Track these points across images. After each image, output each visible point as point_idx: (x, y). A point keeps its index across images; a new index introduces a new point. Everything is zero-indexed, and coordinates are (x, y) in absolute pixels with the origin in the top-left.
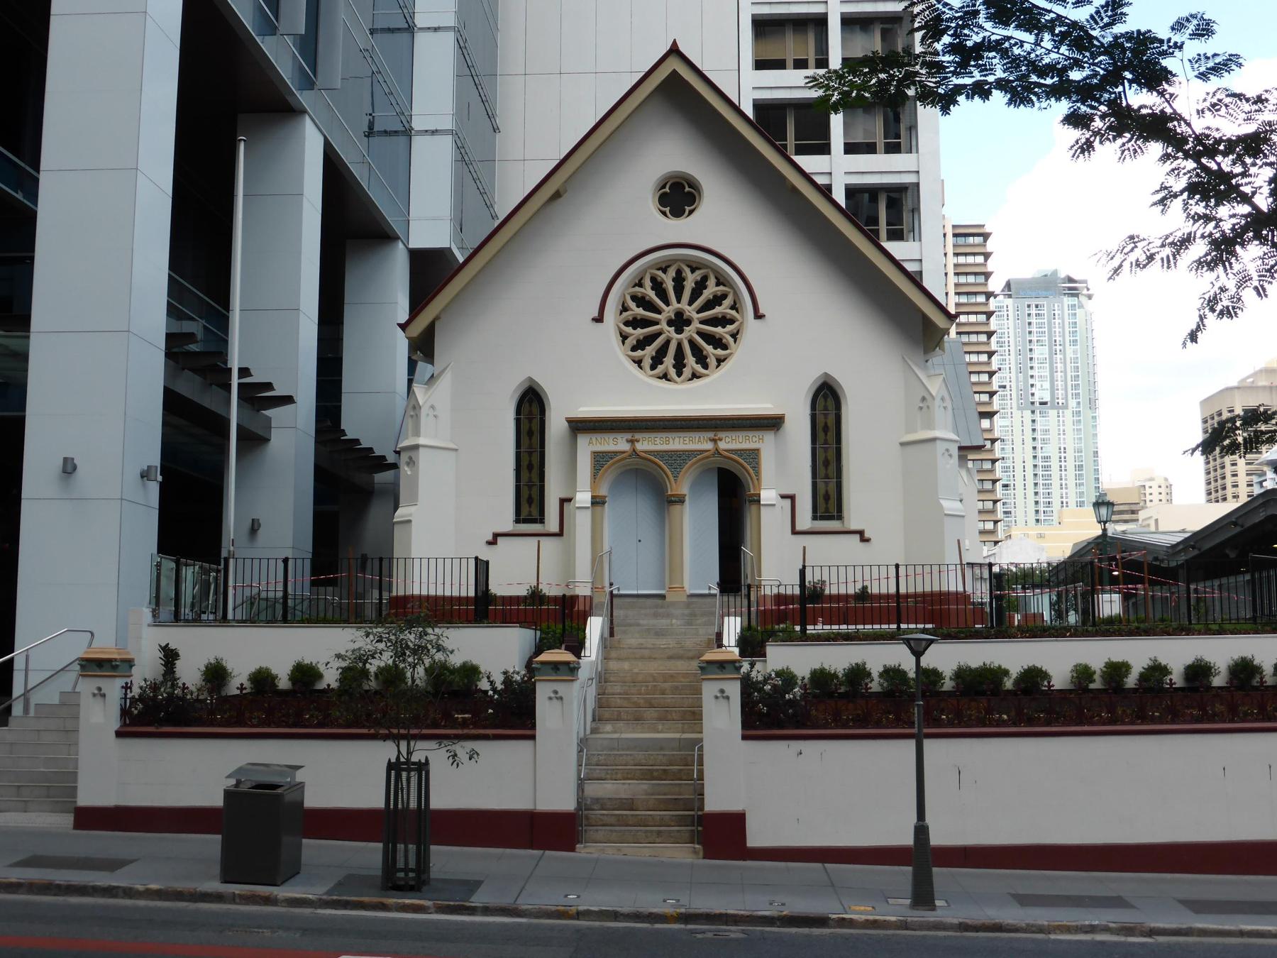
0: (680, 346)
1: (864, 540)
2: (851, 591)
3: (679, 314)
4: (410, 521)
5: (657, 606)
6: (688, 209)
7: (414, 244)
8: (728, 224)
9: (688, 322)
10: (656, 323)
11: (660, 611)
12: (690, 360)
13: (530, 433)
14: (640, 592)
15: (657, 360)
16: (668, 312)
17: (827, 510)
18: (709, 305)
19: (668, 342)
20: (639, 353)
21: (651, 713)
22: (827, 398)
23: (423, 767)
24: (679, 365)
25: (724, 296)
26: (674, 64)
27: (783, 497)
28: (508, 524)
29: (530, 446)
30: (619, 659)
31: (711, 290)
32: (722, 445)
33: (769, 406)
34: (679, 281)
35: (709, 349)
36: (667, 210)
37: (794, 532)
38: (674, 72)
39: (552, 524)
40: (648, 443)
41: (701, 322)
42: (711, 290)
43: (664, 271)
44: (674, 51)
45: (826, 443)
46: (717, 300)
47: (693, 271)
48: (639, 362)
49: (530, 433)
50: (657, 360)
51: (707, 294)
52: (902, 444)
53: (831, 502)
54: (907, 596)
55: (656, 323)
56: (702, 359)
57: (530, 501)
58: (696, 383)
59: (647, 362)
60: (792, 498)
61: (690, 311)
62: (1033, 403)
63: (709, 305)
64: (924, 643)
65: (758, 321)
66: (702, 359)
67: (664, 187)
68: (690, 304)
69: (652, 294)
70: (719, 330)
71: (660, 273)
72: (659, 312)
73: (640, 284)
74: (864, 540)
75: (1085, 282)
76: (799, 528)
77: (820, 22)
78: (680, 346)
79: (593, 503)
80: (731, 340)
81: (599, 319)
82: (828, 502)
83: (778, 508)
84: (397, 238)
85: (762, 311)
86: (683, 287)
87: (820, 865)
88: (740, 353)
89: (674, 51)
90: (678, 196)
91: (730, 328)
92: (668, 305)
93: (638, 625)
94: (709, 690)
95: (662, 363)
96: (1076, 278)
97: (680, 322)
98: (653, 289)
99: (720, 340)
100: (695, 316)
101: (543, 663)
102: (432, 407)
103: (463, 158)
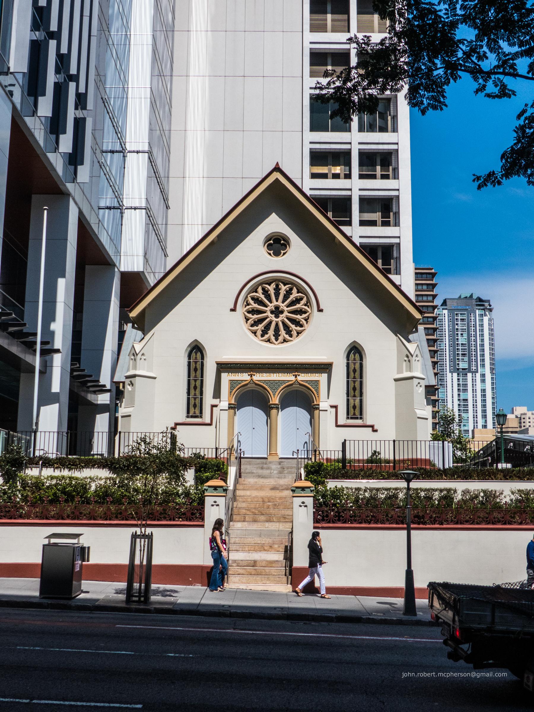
0: (277, 325)
2: (365, 458)
3: (277, 308)
4: (130, 416)
5: (263, 463)
6: (282, 252)
7: (122, 269)
8: (301, 260)
9: (282, 312)
11: (265, 466)
12: (283, 332)
13: (196, 370)
14: (254, 456)
15: (264, 332)
16: (271, 306)
17: (354, 414)
18: (292, 303)
19: (270, 323)
20: (255, 328)
21: (262, 518)
22: (355, 351)
23: (150, 537)
24: (277, 335)
25: (301, 299)
26: (277, 175)
27: (332, 407)
28: (182, 417)
30: (244, 490)
31: (295, 294)
32: (299, 378)
34: (266, 292)
35: (293, 327)
36: (271, 252)
37: (337, 426)
38: (277, 180)
39: (207, 419)
40: (258, 377)
41: (289, 312)
42: (295, 294)
44: (277, 169)
45: (354, 378)
46: (298, 301)
48: (255, 333)
49: (196, 370)
50: (264, 332)
51: (292, 297)
52: (396, 380)
53: (357, 410)
54: (399, 461)
56: (289, 332)
57: (194, 406)
58: (285, 345)
59: (259, 333)
60: (336, 407)
61: (283, 306)
62: (458, 369)
63: (292, 303)
64: (412, 476)
66: (289, 332)
68: (283, 302)
70: (298, 317)
72: (266, 306)
75: (488, 301)
76: (339, 423)
77: (347, 154)
78: (277, 325)
79: (229, 408)
80: (305, 322)
81: (233, 310)
82: (355, 410)
83: (328, 412)
85: (321, 307)
87: (353, 596)
88: (309, 329)
89: (277, 169)
90: (277, 244)
91: (304, 316)
92: (271, 302)
93: (253, 473)
94: (297, 501)
95: (267, 334)
96: (484, 299)
97: (277, 312)
99: (299, 322)
100: (286, 309)
101: (209, 487)
103: (151, 221)
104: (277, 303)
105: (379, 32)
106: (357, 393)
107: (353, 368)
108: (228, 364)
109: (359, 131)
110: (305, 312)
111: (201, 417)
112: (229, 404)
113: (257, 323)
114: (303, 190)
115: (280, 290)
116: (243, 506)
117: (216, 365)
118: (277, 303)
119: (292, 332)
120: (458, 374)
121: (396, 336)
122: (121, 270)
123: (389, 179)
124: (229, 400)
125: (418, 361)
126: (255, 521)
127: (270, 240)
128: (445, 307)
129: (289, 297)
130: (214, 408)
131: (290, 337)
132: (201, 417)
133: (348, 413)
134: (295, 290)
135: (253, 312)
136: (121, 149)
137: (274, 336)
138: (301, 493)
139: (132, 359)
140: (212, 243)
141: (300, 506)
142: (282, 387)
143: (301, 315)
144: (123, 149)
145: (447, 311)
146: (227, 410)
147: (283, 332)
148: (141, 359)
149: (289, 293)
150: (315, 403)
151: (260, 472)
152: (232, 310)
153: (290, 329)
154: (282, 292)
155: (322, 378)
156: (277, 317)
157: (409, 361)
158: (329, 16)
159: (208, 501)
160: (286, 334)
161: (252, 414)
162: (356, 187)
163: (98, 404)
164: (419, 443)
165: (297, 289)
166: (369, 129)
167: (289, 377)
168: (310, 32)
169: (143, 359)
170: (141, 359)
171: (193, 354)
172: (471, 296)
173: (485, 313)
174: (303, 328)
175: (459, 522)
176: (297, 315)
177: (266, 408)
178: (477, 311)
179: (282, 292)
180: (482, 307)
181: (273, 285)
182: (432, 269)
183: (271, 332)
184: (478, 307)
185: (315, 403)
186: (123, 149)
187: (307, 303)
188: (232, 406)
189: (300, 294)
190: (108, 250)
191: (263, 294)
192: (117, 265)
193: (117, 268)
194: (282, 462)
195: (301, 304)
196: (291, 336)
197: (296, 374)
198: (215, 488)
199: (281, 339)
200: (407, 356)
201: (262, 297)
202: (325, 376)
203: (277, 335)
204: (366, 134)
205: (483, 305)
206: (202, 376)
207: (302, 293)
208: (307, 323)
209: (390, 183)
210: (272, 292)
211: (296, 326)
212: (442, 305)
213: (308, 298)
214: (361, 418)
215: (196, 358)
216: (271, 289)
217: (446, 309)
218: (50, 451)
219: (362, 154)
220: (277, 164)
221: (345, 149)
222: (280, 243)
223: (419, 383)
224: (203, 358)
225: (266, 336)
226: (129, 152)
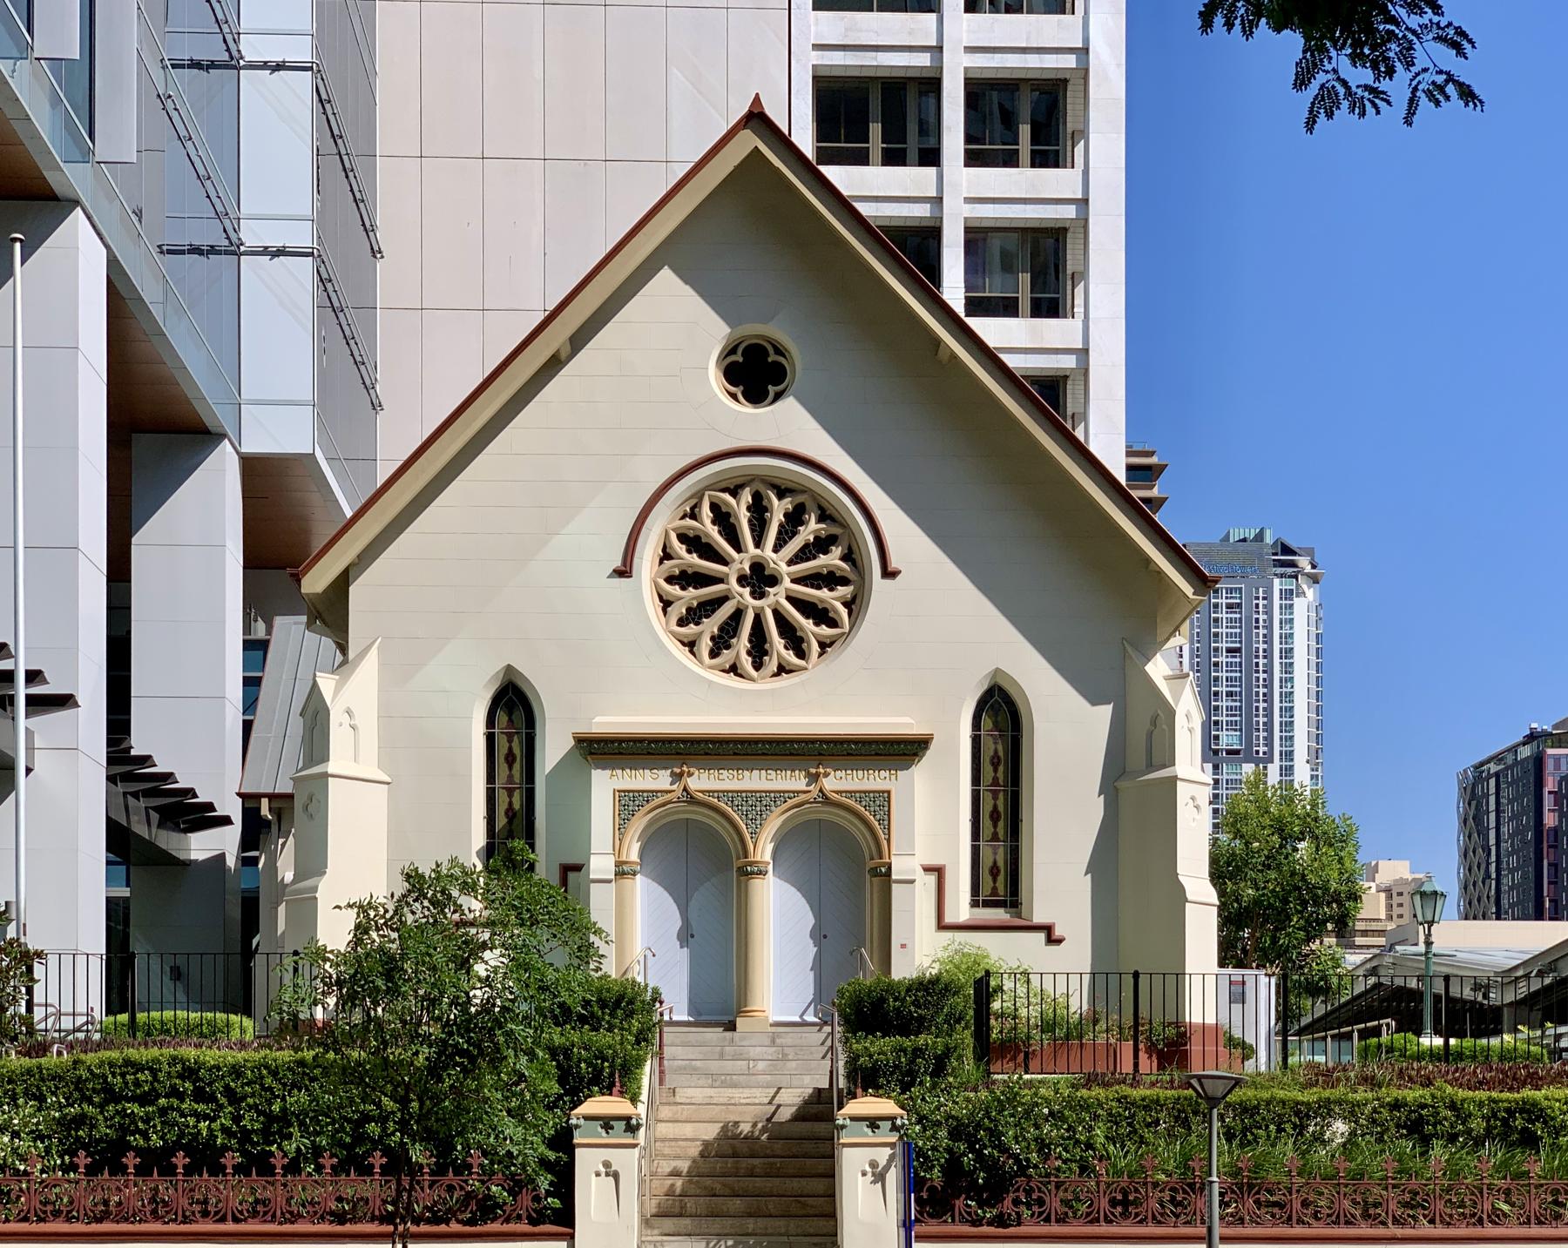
1: (1052, 940)
7: (246, 448)
9: (774, 581)
10: (758, 543)
16: (741, 563)
17: (994, 891)
18: (804, 554)
19: (738, 615)
22: (1001, 713)
27: (927, 869)
29: (510, 778)
36: (738, 358)
37: (942, 926)
40: (702, 781)
43: (734, 493)
47: (780, 497)
50: (721, 642)
55: (758, 543)
60: (938, 871)
61: (778, 562)
62: (1216, 752)
65: (888, 582)
67: (733, 351)
69: (713, 532)
70: (824, 593)
71: (727, 497)
73: (693, 515)
74: (1052, 940)
75: (1310, 552)
81: (624, 572)
84: (223, 436)
85: (894, 563)
96: (1293, 544)
98: (714, 522)
100: (787, 583)
102: (349, 712)
108: (813, 741)
109: (967, 11)
112: (618, 864)
120: (1216, 767)
122: (244, 450)
130: (571, 876)
135: (686, 579)
136: (226, 57)
138: (866, 1135)
146: (609, 881)
149: (830, 580)
151: (715, 1066)
156: (758, 594)
159: (587, 1162)
162: (965, 192)
163: (187, 864)
172: (1260, 537)
175: (1342, 1219)
176: (819, 588)
178: (1277, 581)
180: (1290, 570)
182: (1151, 454)
184: (1282, 570)
194: (779, 1035)
198: (607, 1122)
209: (1053, 331)
218: (67, 1007)
219: (978, 90)
220: (757, 99)
224: (530, 722)
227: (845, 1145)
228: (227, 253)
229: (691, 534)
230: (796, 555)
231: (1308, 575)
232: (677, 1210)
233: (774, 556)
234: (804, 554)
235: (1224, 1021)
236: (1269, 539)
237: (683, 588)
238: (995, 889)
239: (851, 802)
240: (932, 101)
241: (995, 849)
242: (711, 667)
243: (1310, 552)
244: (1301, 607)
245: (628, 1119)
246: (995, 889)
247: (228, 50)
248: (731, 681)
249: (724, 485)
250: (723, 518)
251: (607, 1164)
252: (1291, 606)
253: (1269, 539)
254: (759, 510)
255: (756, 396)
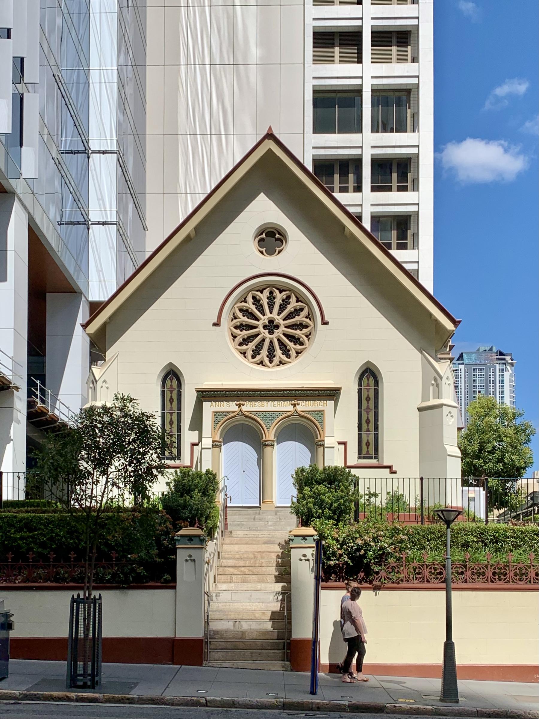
0: (271, 342)
3: (271, 321)
6: (278, 249)
8: (303, 259)
9: (277, 327)
12: (278, 352)
14: (244, 505)
15: (256, 352)
16: (264, 320)
17: (368, 452)
18: (290, 316)
19: (257, 319)
22: (369, 375)
24: (271, 356)
25: (302, 310)
27: (340, 443)
31: (293, 304)
32: (299, 408)
33: (331, 382)
38: (270, 151)
40: (249, 407)
42: (293, 304)
44: (270, 136)
46: (297, 312)
47: (281, 292)
50: (256, 352)
51: (290, 308)
52: (420, 409)
59: (250, 353)
61: (279, 319)
63: (290, 316)
66: (286, 351)
68: (279, 314)
73: (245, 301)
78: (271, 342)
79: (213, 446)
80: (306, 339)
85: (327, 319)
86: (261, 306)
89: (270, 136)
90: (271, 239)
97: (271, 326)
99: (299, 339)
100: (282, 322)
101: (182, 536)
104: (271, 315)
105: (398, 4)
106: (371, 426)
107: (366, 396)
110: (306, 327)
111: (179, 459)
112: (213, 441)
113: (246, 341)
114: (305, 165)
115: (274, 298)
116: (229, 564)
117: (195, 394)
118: (271, 315)
119: (290, 352)
121: (421, 353)
123: (407, 190)
124: (213, 436)
125: (449, 384)
126: (244, 582)
127: (262, 234)
128: (461, 362)
129: (286, 308)
130: (195, 447)
131: (287, 357)
132: (179, 459)
133: (360, 452)
134: (293, 299)
135: (242, 327)
137: (267, 356)
138: (301, 544)
139: (91, 388)
140: (188, 239)
141: (301, 560)
142: (278, 419)
143: (301, 330)
144: (86, 149)
145: (463, 366)
146: (210, 449)
147: (278, 352)
148: (102, 387)
149: (286, 302)
150: (319, 439)
151: (251, 523)
152: (215, 325)
153: (288, 347)
154: (278, 301)
155: (327, 406)
156: (271, 333)
157: (438, 385)
158: (337, 49)
160: (283, 354)
161: (240, 451)
164: (448, 481)
165: (296, 297)
166: (383, 130)
167: (286, 406)
168: (314, 5)
169: (104, 388)
170: (102, 387)
171: (168, 382)
172: (491, 349)
173: (506, 368)
174: (304, 347)
176: (296, 330)
177: (260, 445)
178: (497, 365)
179: (278, 301)
180: (503, 361)
181: (266, 293)
183: (264, 352)
185: (319, 439)
186: (86, 149)
187: (309, 314)
188: (217, 443)
189: (300, 303)
190: (50, 242)
191: (253, 304)
192: (83, 291)
193: (85, 297)
194: (278, 511)
195: (301, 316)
196: (289, 357)
197: (296, 402)
198: (190, 538)
199: (276, 360)
200: (435, 380)
201: (253, 308)
202: (331, 403)
203: (271, 356)
204: (380, 135)
205: (504, 359)
206: (180, 408)
207: (302, 302)
208: (309, 340)
210: (265, 302)
211: (295, 344)
212: (458, 360)
213: (309, 308)
214: (376, 458)
215: (171, 386)
216: (264, 297)
217: (463, 364)
220: (270, 128)
221: (355, 155)
222: (275, 237)
223: (450, 412)
224: (180, 385)
225: (258, 358)
226: (93, 152)
227: (292, 548)
228: (83, 224)
229: (245, 308)
230: (287, 317)
231: (509, 363)
232: (229, 581)
233: (278, 317)
234: (282, 308)
235: (466, 506)
236: (495, 350)
237: (241, 331)
238: (368, 452)
239: (308, 416)
240: (381, 219)
241: (368, 435)
242: (252, 363)
243: (510, 355)
244: (507, 375)
245: (199, 536)
246: (368, 452)
247: (84, 146)
248: (260, 367)
249: (257, 289)
250: (256, 301)
251: (190, 556)
252: (503, 375)
253: (495, 350)
254: (271, 298)
255: (271, 252)
